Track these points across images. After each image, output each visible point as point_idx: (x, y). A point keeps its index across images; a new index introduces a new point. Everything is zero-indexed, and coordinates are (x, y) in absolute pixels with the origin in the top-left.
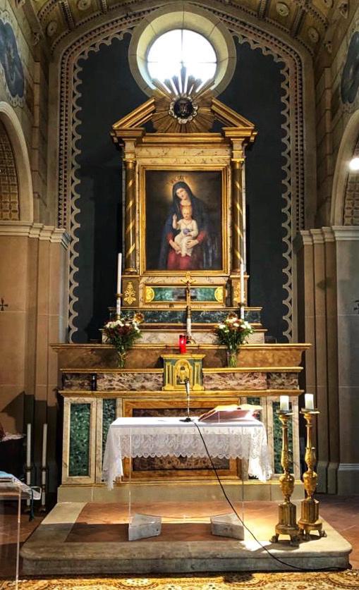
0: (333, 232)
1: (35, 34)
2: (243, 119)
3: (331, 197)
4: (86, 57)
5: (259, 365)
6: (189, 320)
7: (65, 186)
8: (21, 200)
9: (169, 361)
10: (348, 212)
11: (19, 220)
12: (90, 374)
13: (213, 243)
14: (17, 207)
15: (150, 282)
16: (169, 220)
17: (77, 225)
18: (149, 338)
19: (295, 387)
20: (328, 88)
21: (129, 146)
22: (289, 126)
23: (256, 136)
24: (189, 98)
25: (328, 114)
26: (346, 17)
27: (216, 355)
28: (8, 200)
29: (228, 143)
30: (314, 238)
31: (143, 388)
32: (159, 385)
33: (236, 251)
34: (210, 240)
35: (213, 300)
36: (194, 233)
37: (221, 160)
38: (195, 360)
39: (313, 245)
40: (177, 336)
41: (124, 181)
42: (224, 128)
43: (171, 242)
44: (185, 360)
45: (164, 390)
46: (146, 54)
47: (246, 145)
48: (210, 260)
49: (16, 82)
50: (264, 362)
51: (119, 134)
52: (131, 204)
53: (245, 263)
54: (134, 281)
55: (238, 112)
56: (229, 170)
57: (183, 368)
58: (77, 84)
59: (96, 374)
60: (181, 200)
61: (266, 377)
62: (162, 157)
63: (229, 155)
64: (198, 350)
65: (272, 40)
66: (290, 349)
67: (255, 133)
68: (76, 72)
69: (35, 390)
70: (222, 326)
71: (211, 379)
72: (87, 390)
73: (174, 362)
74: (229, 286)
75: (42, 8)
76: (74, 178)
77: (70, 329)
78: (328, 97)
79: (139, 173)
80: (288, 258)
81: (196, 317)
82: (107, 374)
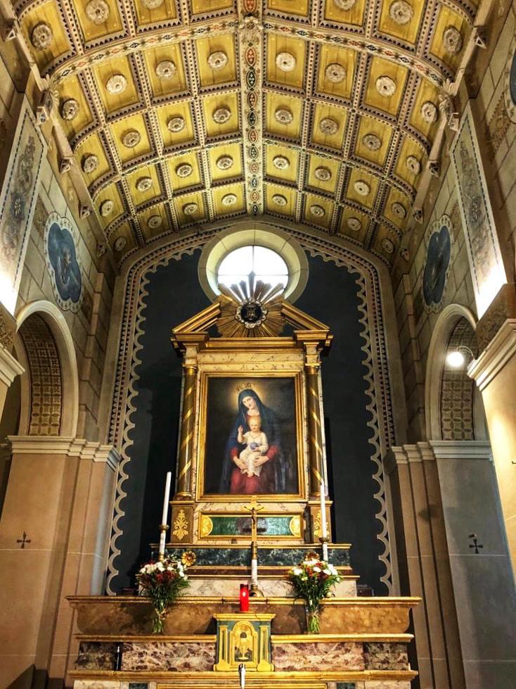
0: (431, 448)
1: (101, 246)
2: (316, 322)
3: (424, 408)
4: (154, 271)
5: (351, 629)
6: (254, 562)
7: (121, 398)
8: (64, 414)
9: (225, 623)
10: (446, 425)
11: (59, 435)
12: (114, 643)
13: (286, 459)
14: (58, 419)
15: (207, 510)
16: (234, 433)
17: (130, 442)
18: (202, 587)
19: (405, 666)
20: (408, 294)
21: (191, 352)
22: (368, 334)
23: (332, 340)
24: (257, 302)
25: (411, 320)
26: (421, 223)
27: (291, 614)
28: (49, 413)
29: (300, 347)
30: (409, 455)
31: (187, 666)
32: (209, 661)
33: (314, 469)
34: (282, 456)
35: (288, 534)
36: (264, 448)
37: (294, 367)
38: (261, 623)
39: (409, 464)
40: (238, 583)
41: (183, 390)
42: (295, 331)
43: (235, 459)
44: (247, 623)
45: (216, 671)
46: (217, 268)
47: (321, 349)
48: (284, 482)
49: (69, 287)
50: (357, 626)
51: (180, 338)
52: (189, 414)
53: (327, 485)
54: (186, 508)
55: (310, 314)
56: (303, 376)
57: (243, 635)
58: (143, 295)
59: (122, 643)
60: (248, 409)
61: (362, 651)
62: (227, 363)
63: (302, 360)
64: (266, 607)
65: (345, 253)
66: (393, 606)
67: (331, 337)
68: (143, 284)
69: (50, 661)
70: (297, 571)
71: (284, 652)
72: (108, 669)
73: (231, 625)
74: (308, 516)
75: (110, 224)
76: (132, 390)
77: (109, 572)
78: (409, 301)
79: (200, 380)
80: (379, 480)
81: (264, 557)
82: (136, 643)
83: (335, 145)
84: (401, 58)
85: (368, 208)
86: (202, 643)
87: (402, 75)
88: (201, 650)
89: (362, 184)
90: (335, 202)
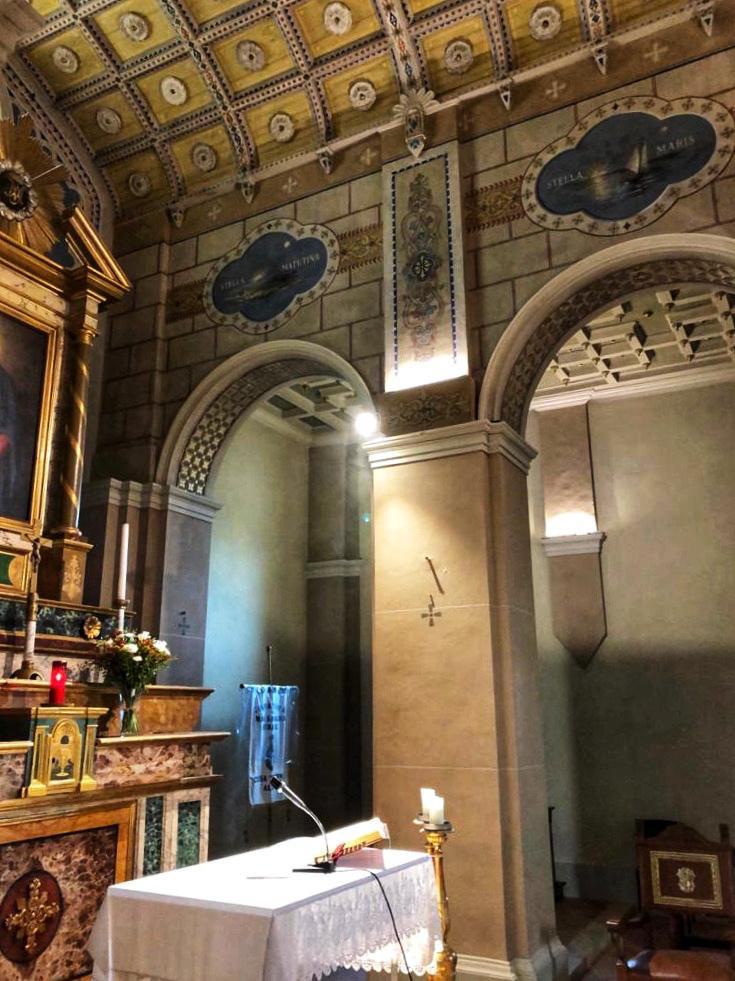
32: (14, 783)
83: (198, 11)
84: (391, 15)
85: (157, 119)
86: (7, 755)
87: (370, 27)
88: (5, 767)
89: (182, 87)
90: (116, 75)
